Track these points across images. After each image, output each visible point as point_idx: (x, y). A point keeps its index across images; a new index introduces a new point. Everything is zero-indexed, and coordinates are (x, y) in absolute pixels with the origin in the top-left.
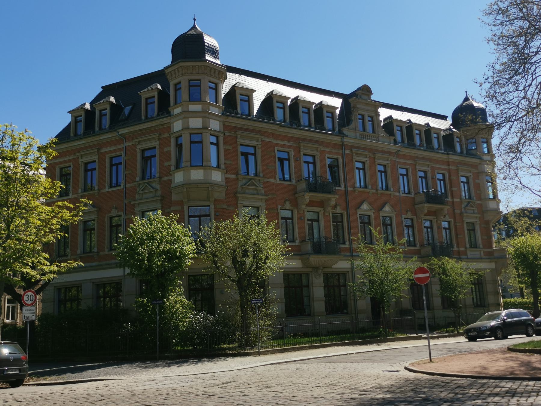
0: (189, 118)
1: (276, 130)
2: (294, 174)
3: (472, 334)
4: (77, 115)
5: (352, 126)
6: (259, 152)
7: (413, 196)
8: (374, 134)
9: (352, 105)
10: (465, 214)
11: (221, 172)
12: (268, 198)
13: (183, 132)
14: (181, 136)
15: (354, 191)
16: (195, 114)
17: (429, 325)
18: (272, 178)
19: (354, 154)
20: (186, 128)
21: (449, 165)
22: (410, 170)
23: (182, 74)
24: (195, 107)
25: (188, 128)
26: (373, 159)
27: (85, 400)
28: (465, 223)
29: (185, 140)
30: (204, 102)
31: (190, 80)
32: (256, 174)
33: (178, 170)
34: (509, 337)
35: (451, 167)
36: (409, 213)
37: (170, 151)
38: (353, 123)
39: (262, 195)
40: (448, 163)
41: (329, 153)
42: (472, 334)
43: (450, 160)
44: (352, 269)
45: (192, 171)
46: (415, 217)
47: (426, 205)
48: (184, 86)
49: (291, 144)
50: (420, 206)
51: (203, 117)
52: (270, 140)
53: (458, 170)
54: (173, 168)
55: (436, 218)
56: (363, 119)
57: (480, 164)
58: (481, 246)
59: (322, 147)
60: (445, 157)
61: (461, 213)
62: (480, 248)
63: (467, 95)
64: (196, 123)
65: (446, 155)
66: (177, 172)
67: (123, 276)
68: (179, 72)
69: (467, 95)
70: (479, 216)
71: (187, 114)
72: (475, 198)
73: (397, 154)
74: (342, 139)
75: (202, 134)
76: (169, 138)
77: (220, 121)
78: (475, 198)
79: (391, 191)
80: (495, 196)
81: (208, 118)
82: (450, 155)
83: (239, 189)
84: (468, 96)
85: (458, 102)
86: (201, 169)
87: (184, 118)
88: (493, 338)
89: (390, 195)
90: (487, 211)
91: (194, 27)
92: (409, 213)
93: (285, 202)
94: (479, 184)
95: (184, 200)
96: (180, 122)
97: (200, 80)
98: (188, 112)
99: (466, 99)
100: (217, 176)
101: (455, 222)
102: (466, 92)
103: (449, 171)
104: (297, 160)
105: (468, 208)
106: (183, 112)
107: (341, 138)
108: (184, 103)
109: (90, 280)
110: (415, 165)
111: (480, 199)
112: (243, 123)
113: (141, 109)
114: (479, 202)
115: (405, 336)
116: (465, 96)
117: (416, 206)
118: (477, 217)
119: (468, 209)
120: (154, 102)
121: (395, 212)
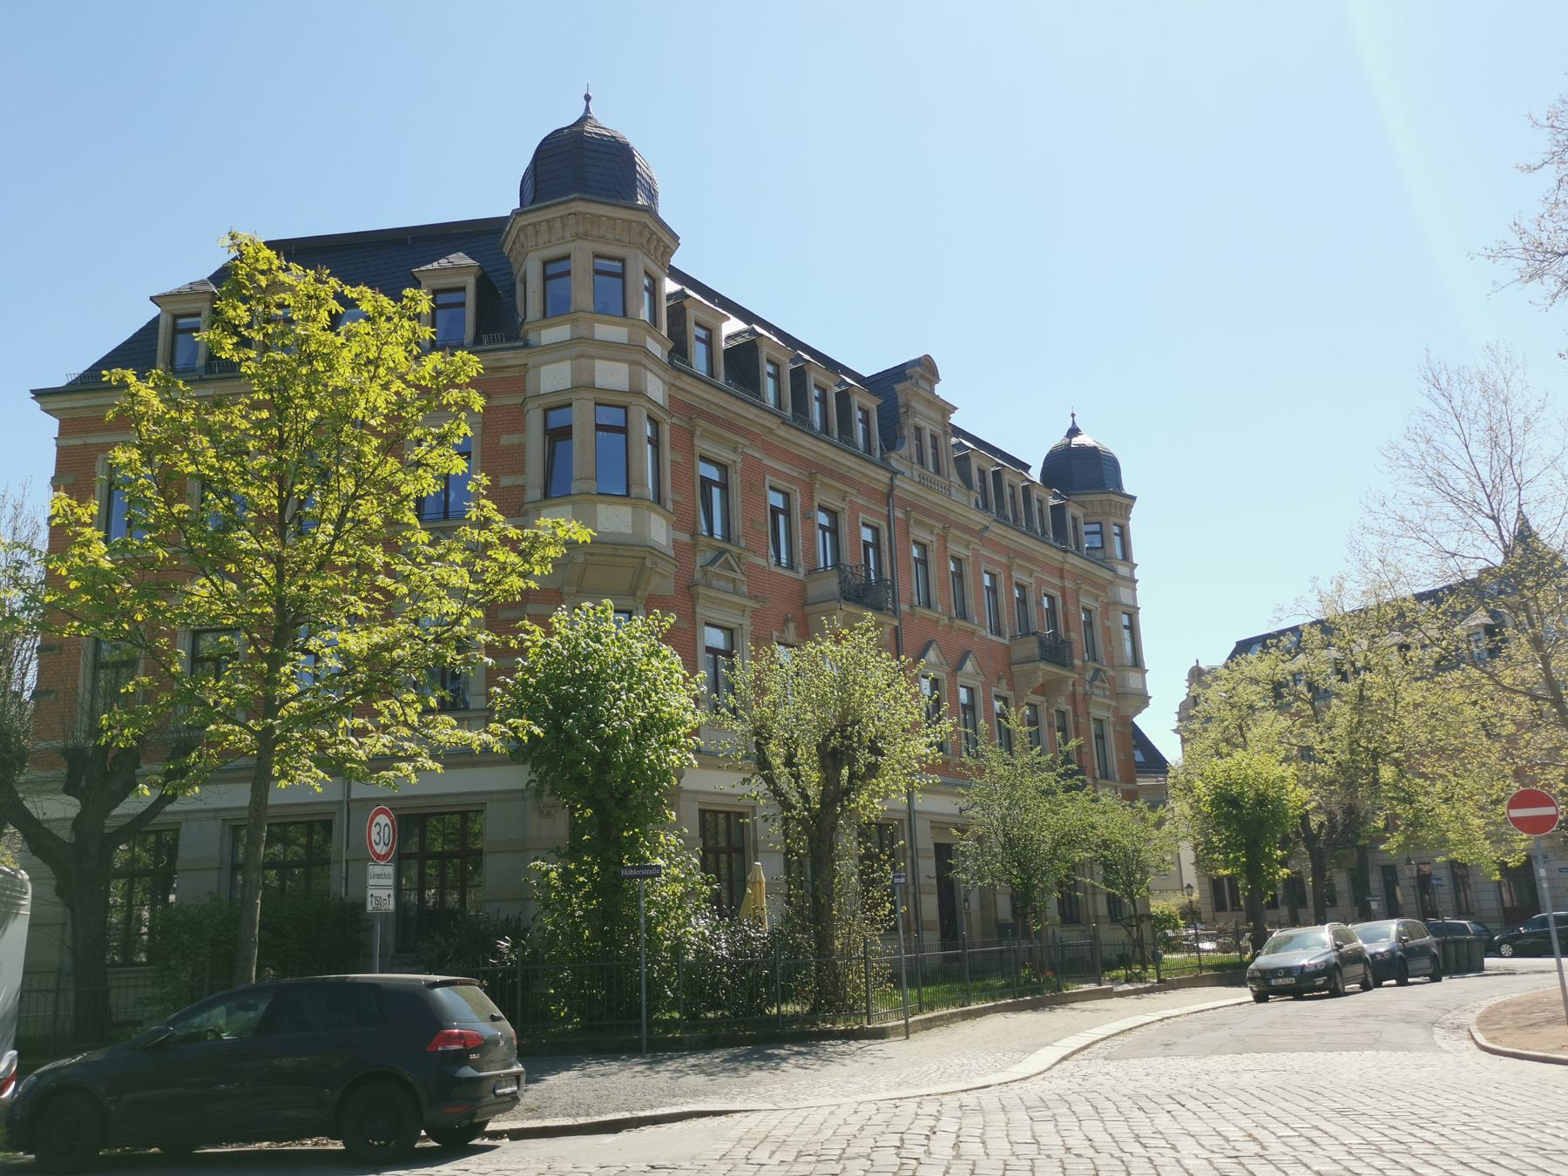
0: (593, 358)
1: (771, 431)
2: (801, 553)
3: (1280, 981)
4: (182, 312)
5: (904, 451)
6: (735, 481)
7: (1006, 642)
8: (937, 478)
9: (901, 400)
10: (1094, 698)
11: (667, 519)
12: (757, 606)
13: (573, 396)
14: (570, 405)
15: (913, 615)
16: (611, 350)
17: (907, 972)
18: (762, 556)
19: (912, 522)
20: (584, 385)
21: (1062, 578)
22: (1002, 579)
23: (577, 235)
24: (609, 331)
25: (591, 387)
26: (944, 539)
27: (1499, 1122)
28: (1091, 718)
29: (582, 417)
30: (636, 322)
31: (597, 256)
32: (727, 536)
33: (549, 502)
34: (1384, 983)
35: (1068, 584)
36: (1004, 682)
37: (521, 448)
38: (906, 443)
39: (742, 595)
40: (1061, 574)
41: (865, 509)
42: (1280, 981)
43: (1067, 567)
44: (910, 814)
45: (601, 508)
46: (1012, 693)
47: (1042, 666)
48: (581, 265)
49: (795, 474)
50: (1027, 667)
51: (632, 363)
52: (758, 456)
53: (1077, 592)
54: (535, 493)
55: (1047, 701)
56: (919, 438)
57: (1111, 582)
58: (1118, 777)
59: (854, 492)
60: (1058, 556)
61: (1086, 694)
62: (1115, 780)
63: (1074, 422)
64: (612, 375)
65: (1061, 554)
66: (545, 507)
67: (340, 802)
68: (550, 230)
69: (1074, 422)
70: (1114, 703)
71: (583, 348)
72: (1105, 661)
73: (981, 533)
74: (892, 479)
75: (626, 408)
76: (521, 409)
77: (664, 382)
78: (1105, 661)
79: (973, 623)
80: (1137, 663)
81: (644, 366)
82: (1069, 555)
83: (698, 575)
84: (1078, 425)
85: (1056, 438)
86: (626, 504)
87: (581, 356)
88: (1394, 982)
89: (973, 633)
90: (1126, 694)
91: (585, 118)
92: (1004, 682)
93: (786, 621)
94: (1109, 629)
95: (566, 589)
96: (566, 367)
97: (622, 260)
98: (591, 340)
99: (1074, 432)
100: (659, 531)
101: (1076, 715)
102: (1073, 415)
103: (1063, 590)
104: (808, 517)
105: (1098, 683)
106: (575, 340)
107: (889, 475)
108: (583, 314)
109: (216, 810)
110: (1009, 568)
111: (1113, 666)
112: (709, 397)
113: (155, 351)
114: (1111, 673)
115: (1086, 987)
116: (1070, 426)
117: (1014, 668)
118: (1109, 707)
119: (1097, 687)
120: (463, 304)
121: (982, 678)
